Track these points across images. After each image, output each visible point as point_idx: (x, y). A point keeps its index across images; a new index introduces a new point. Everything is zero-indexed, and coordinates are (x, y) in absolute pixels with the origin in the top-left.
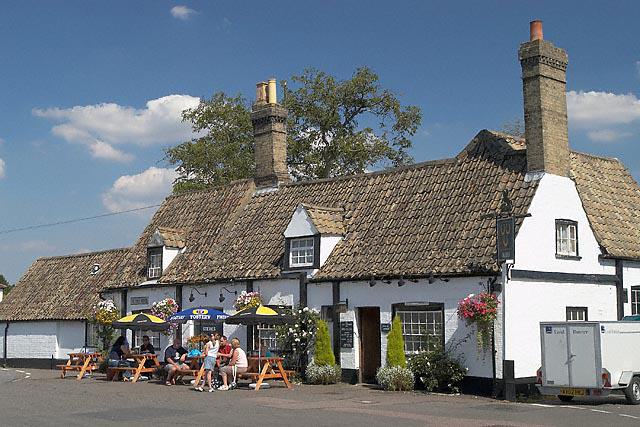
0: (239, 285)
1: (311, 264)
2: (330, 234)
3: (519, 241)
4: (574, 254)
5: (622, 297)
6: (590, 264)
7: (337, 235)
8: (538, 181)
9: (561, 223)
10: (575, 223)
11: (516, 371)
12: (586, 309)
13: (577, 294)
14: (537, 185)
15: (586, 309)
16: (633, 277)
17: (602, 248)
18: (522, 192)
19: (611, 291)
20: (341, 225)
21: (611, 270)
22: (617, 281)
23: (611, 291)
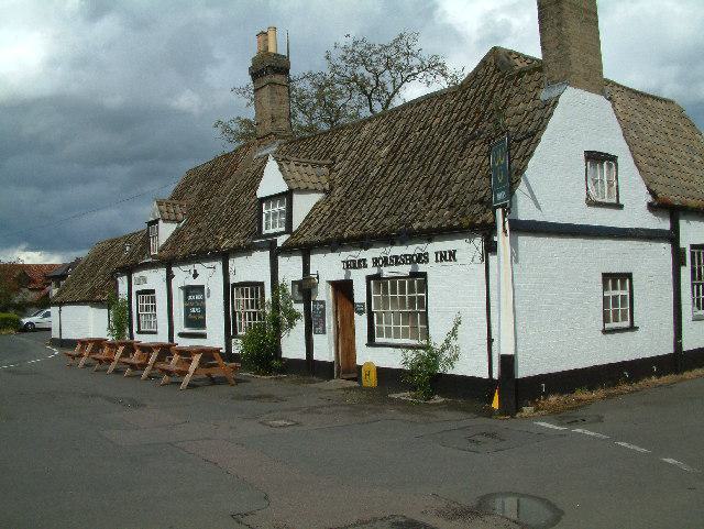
0: (58, 299)
1: (283, 229)
2: (307, 191)
3: (87, 307)
4: (614, 201)
5: (678, 258)
6: (636, 214)
7: (316, 191)
8: (559, 96)
9: (594, 158)
10: (613, 159)
11: (477, 375)
12: (629, 276)
13: (615, 255)
14: (556, 102)
15: (629, 276)
16: (693, 233)
17: (653, 193)
18: (538, 114)
19: (664, 249)
20: (324, 179)
21: (666, 225)
22: (672, 237)
23: (664, 249)
